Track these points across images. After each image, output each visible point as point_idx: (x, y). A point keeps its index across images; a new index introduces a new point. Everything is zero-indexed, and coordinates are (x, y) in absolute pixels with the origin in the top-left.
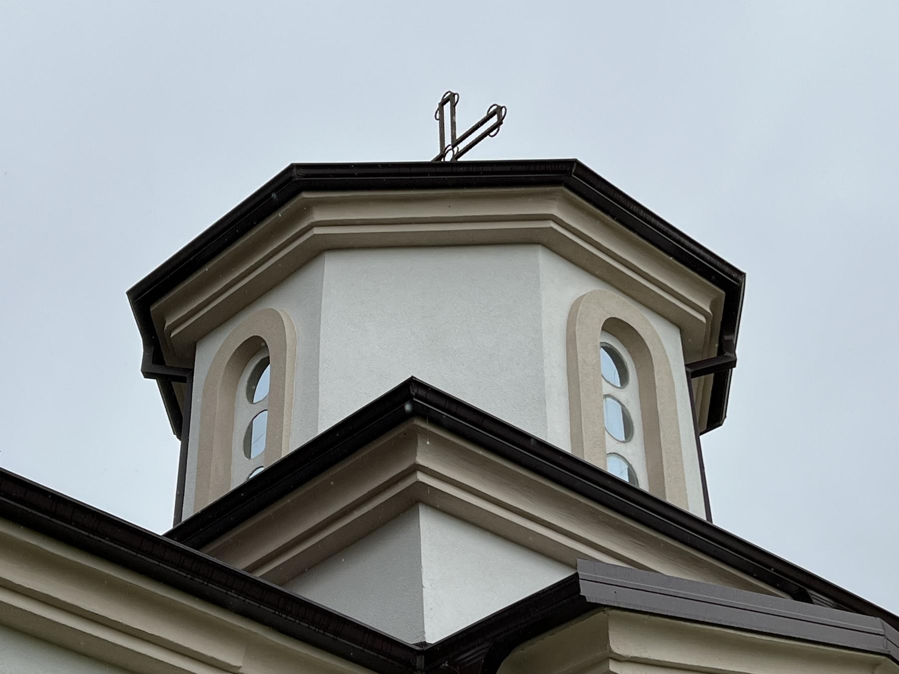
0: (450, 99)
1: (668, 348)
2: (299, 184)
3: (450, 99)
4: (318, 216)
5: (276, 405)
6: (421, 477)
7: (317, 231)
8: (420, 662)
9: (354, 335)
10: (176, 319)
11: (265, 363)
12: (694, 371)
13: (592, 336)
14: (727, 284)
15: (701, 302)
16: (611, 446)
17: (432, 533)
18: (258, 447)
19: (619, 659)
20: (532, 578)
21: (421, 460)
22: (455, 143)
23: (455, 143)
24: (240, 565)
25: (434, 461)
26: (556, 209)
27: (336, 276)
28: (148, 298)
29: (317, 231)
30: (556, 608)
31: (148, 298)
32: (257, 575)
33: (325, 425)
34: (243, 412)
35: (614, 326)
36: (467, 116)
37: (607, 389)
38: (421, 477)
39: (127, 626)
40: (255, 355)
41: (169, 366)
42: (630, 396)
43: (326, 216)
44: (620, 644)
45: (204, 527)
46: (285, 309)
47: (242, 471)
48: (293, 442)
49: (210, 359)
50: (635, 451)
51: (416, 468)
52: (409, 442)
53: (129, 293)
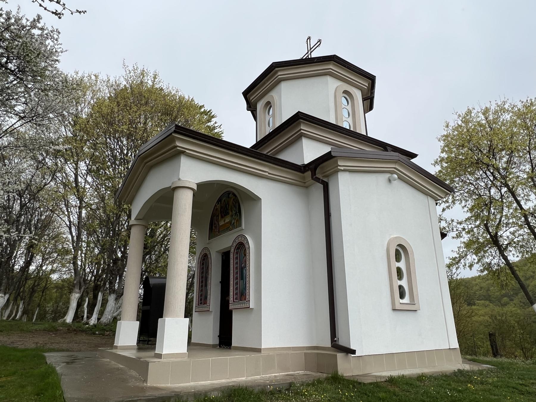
0: (309, 38)
1: (358, 95)
2: (275, 67)
3: (309, 38)
4: (279, 74)
5: (274, 116)
6: (302, 131)
7: (279, 77)
8: (302, 168)
9: (291, 99)
10: (252, 98)
11: (271, 107)
12: (364, 100)
13: (340, 93)
14: (371, 79)
15: (365, 84)
16: (344, 119)
17: (305, 142)
18: (271, 125)
19: (340, 166)
20: (324, 149)
21: (302, 128)
22: (311, 49)
23: (311, 49)
24: (265, 153)
25: (304, 128)
26: (331, 67)
27: (284, 86)
28: (246, 94)
29: (279, 77)
30: (327, 157)
31: (246, 94)
32: (268, 154)
33: (284, 120)
34: (267, 118)
35: (345, 92)
36: (313, 42)
37: (343, 106)
38: (302, 131)
39: (159, 284)
40: (269, 105)
41: (252, 107)
42: (349, 107)
43: (281, 73)
44: (340, 163)
45: (259, 144)
46: (274, 94)
47: (269, 130)
48: (277, 125)
49: (260, 106)
50: (350, 120)
51: (301, 129)
52: (299, 124)
53: (243, 93)
